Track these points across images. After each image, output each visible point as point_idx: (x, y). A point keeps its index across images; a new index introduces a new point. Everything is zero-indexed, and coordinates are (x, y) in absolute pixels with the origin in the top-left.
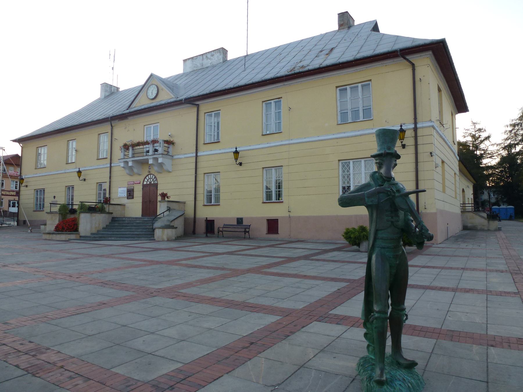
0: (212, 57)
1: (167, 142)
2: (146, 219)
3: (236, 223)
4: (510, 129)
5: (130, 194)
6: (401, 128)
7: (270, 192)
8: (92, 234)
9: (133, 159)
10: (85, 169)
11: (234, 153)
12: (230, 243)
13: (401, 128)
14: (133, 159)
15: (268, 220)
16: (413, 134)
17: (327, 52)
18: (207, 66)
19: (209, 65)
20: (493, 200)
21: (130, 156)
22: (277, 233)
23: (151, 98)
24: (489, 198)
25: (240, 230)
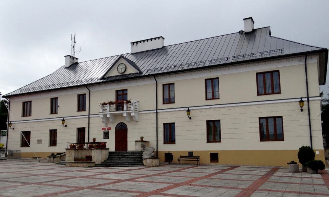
6: (188, 109)
8: (102, 163)
11: (187, 111)
13: (188, 109)
21: (108, 110)
23: (121, 72)
25: (191, 159)
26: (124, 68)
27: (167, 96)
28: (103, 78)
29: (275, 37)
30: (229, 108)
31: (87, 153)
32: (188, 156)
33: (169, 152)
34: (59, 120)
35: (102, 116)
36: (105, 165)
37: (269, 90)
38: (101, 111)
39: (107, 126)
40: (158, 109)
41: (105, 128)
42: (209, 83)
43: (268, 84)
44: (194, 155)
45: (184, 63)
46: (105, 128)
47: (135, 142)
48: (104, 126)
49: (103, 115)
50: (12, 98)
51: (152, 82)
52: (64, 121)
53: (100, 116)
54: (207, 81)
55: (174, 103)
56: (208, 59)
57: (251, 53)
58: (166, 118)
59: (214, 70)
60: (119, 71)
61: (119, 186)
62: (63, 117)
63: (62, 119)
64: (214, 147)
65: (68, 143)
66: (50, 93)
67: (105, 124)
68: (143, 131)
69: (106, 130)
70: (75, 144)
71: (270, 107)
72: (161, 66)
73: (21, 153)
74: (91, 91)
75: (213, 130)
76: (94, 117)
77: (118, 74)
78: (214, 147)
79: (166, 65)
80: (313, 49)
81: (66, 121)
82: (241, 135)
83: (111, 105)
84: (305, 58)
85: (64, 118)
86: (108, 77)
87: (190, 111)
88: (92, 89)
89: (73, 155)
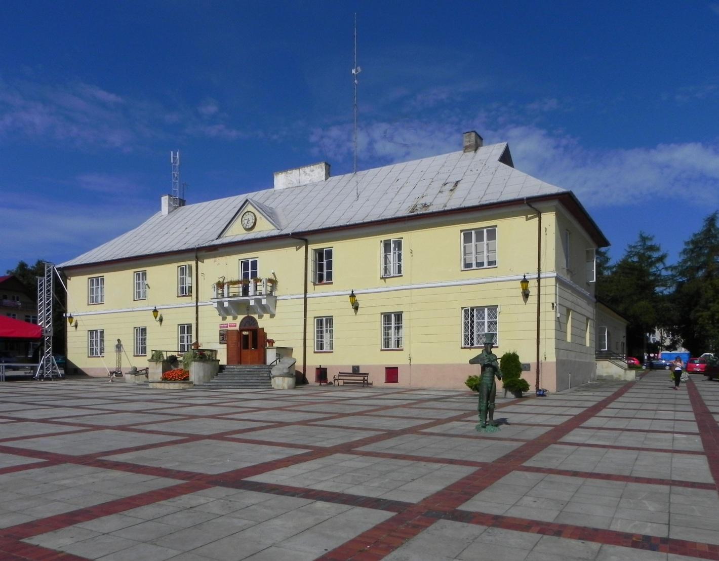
0: (311, 173)
1: (270, 281)
2: (256, 367)
3: (351, 371)
4: (691, 246)
5: (223, 338)
6: (525, 278)
7: (388, 338)
9: (230, 299)
10: (162, 307)
12: (357, 390)
13: (525, 278)
14: (230, 299)
15: (387, 368)
16: (537, 284)
17: (451, 188)
18: (305, 184)
19: (308, 182)
20: (667, 342)
22: (397, 381)
23: (247, 227)
24: (662, 339)
33: (320, 366)
47: (148, 362)
49: (218, 302)
58: (317, 309)
61: (236, 416)
64: (392, 359)
65: (152, 350)
70: (175, 354)
83: (231, 286)
87: (355, 296)
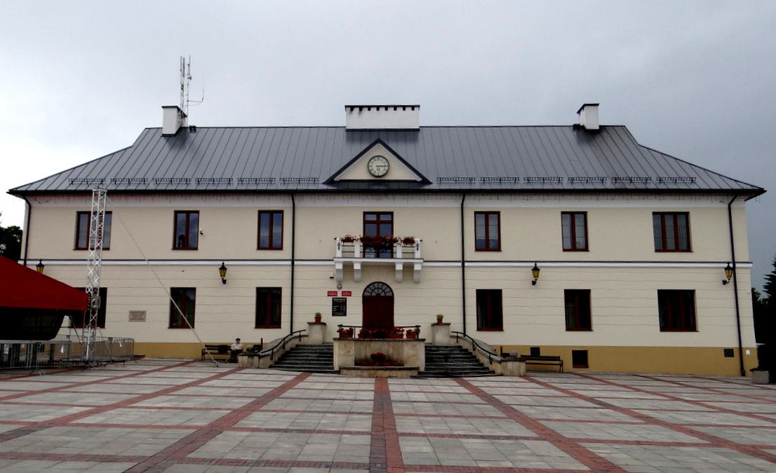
23: (377, 174)
25: (537, 361)
26: (385, 166)
27: (482, 236)
28: (330, 181)
29: (671, 157)
30: (684, 270)
31: (362, 347)
32: (530, 354)
34: (527, 267)
35: (340, 266)
36: (434, 374)
37: (671, 243)
38: (339, 254)
39: (341, 288)
40: (295, 258)
41: (336, 292)
42: (266, 217)
43: (673, 235)
44: (542, 354)
45: (149, 177)
46: (336, 292)
48: (333, 286)
50: (38, 198)
51: (453, 204)
52: (539, 270)
53: (334, 266)
54: (262, 215)
55: (196, 249)
56: (195, 177)
57: (210, 177)
58: (482, 279)
59: (649, 198)
60: (373, 172)
62: (536, 262)
63: (533, 264)
64: (579, 339)
66: (118, 198)
67: (336, 284)
68: (430, 304)
69: (340, 295)
71: (677, 274)
72: (101, 176)
73: (133, 343)
74: (32, 204)
75: (578, 309)
76: (476, 267)
77: (367, 177)
78: (579, 339)
79: (112, 176)
80: (746, 187)
81: (541, 270)
82: (625, 319)
84: (462, 197)
85: (226, 263)
86: (342, 181)
87: (539, 270)
88: (304, 204)
89: (352, 352)
